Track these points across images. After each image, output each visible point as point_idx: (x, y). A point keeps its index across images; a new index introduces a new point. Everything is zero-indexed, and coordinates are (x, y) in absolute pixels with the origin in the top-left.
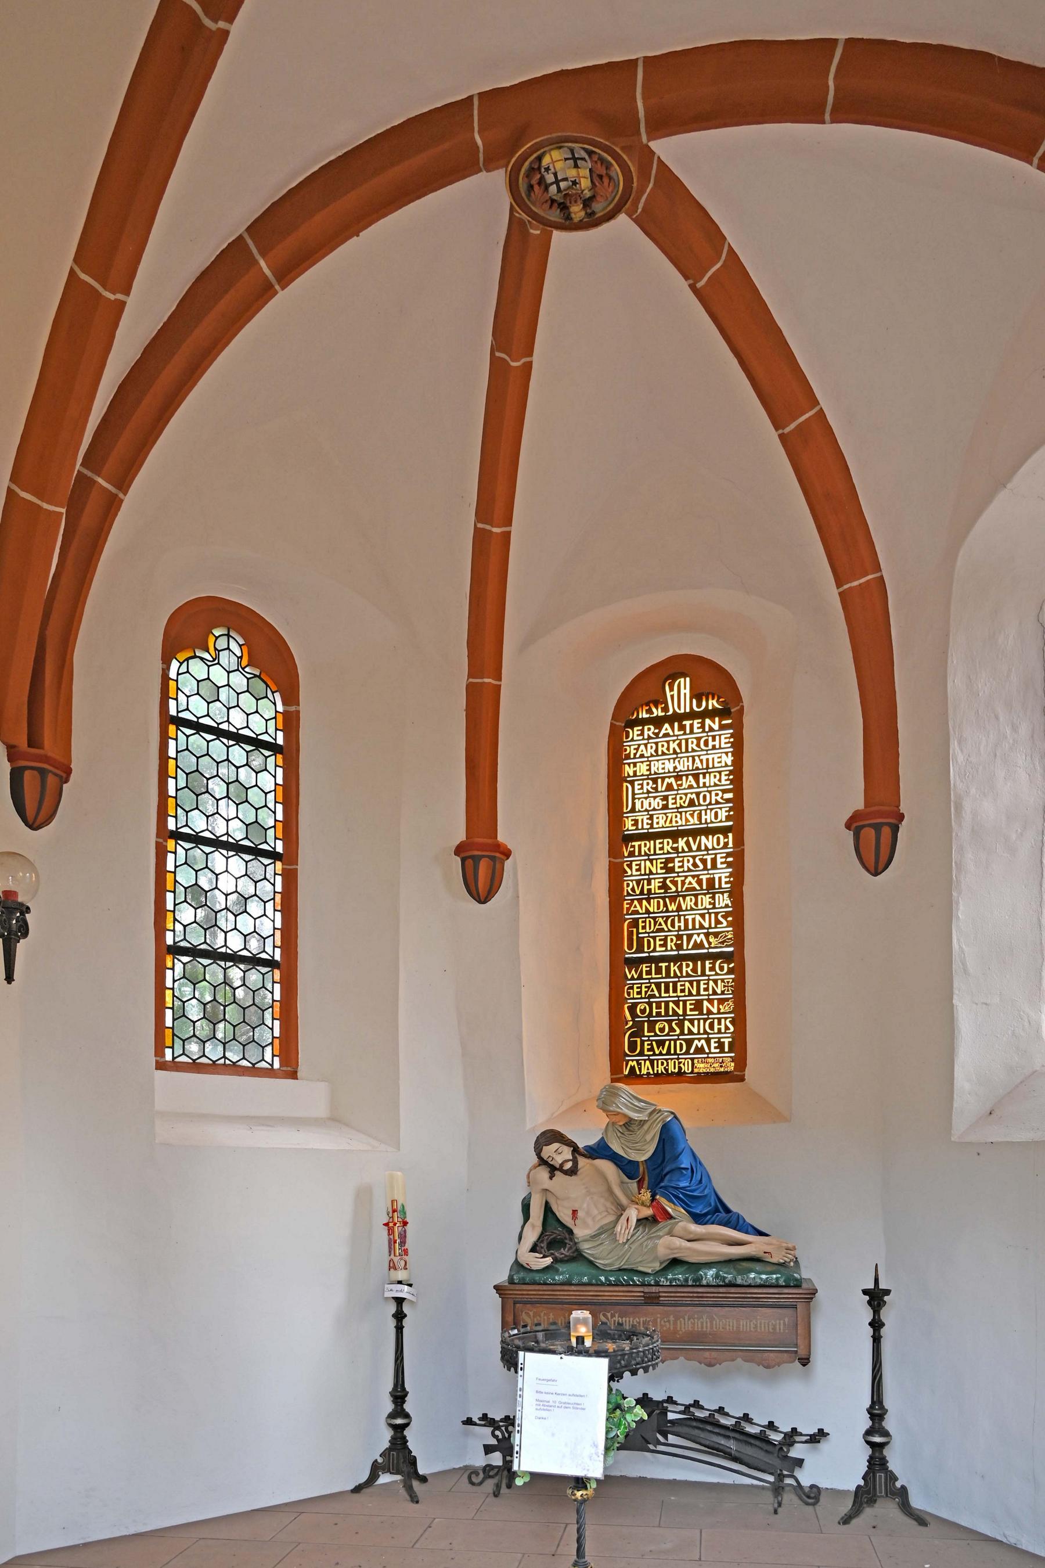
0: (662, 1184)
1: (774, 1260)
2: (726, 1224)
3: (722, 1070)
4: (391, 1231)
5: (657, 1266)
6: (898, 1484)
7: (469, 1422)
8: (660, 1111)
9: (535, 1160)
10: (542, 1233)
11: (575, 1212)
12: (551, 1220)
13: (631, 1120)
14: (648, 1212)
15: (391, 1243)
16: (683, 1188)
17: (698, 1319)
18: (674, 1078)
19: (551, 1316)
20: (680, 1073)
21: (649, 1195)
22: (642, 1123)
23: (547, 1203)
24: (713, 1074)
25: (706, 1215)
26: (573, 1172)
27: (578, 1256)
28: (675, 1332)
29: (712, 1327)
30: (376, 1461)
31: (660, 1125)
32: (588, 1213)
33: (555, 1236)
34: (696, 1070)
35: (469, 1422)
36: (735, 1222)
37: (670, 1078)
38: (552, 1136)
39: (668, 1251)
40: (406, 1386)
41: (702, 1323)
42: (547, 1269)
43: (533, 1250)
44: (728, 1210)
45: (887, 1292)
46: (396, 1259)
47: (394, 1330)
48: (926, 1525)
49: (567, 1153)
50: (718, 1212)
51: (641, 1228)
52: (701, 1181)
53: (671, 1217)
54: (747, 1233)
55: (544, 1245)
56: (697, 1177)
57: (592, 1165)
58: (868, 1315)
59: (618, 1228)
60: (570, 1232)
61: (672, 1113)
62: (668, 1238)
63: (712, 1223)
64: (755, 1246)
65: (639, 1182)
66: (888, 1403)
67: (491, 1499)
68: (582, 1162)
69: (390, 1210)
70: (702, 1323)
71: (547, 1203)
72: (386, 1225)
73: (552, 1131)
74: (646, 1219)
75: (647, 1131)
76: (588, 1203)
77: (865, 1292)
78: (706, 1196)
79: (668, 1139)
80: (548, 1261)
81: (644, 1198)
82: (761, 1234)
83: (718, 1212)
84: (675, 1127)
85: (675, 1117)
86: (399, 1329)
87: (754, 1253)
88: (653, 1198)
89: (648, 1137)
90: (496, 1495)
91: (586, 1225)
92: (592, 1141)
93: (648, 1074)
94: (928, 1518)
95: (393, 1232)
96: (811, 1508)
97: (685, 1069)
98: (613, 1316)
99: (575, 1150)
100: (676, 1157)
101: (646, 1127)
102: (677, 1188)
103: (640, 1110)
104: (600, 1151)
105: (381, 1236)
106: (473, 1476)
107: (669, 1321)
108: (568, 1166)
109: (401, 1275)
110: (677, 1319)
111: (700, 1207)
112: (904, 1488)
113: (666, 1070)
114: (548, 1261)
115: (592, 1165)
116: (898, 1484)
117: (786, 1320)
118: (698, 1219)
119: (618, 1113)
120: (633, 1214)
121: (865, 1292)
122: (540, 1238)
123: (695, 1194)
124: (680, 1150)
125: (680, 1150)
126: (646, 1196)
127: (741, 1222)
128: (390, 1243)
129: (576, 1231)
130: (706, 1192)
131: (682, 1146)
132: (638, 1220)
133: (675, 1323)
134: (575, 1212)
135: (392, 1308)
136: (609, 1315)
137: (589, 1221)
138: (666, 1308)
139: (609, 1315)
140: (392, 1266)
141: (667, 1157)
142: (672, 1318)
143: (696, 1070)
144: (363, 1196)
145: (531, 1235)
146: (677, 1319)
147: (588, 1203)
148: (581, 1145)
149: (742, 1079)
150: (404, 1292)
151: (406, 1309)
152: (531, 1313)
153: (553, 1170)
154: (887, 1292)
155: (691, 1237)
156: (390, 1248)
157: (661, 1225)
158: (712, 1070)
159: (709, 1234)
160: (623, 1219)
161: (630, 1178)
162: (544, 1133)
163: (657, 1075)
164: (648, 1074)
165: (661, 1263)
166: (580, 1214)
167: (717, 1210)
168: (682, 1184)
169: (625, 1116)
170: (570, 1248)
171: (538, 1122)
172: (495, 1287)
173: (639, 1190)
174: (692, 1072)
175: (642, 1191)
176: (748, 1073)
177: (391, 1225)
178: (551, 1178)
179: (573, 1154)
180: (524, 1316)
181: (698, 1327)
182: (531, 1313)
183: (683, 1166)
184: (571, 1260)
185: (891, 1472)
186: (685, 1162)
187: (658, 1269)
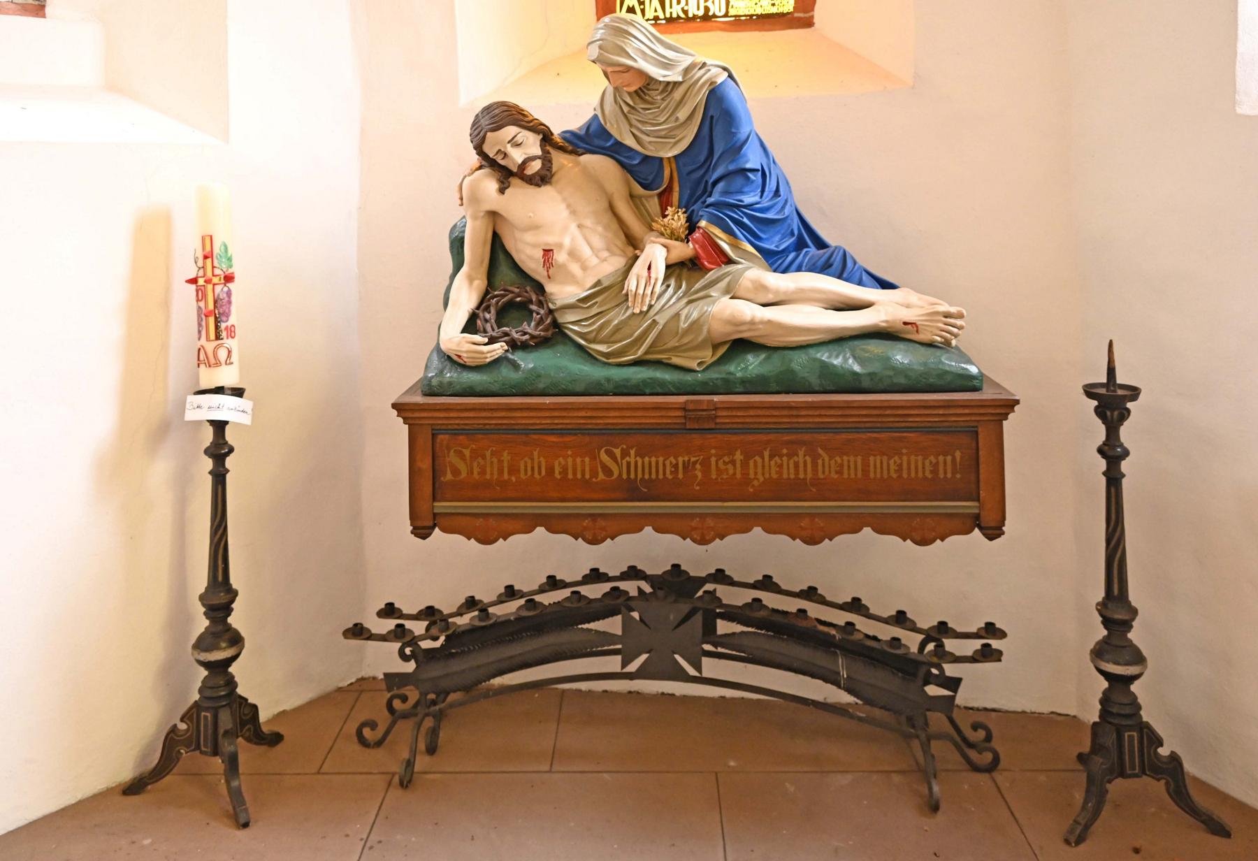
0: (711, 200)
1: (922, 337)
2: (825, 268)
4: (201, 295)
5: (708, 356)
6: (1163, 751)
7: (358, 632)
9: (474, 159)
10: (487, 293)
11: (547, 252)
12: (505, 273)
14: (683, 250)
15: (202, 315)
16: (748, 206)
17: (790, 456)
19: (506, 456)
20: (707, 17)
21: (683, 218)
22: (670, 86)
24: (760, 17)
25: (785, 252)
26: (542, 179)
27: (555, 335)
28: (746, 481)
29: (815, 470)
30: (175, 726)
32: (573, 254)
33: (511, 293)
34: (732, 12)
35: (358, 632)
36: (837, 264)
37: (692, 25)
40: (232, 581)
41: (796, 465)
42: (496, 362)
43: (470, 326)
45: (1134, 393)
46: (210, 347)
47: (209, 480)
48: (1227, 835)
49: (532, 145)
50: (803, 246)
51: (672, 282)
52: (777, 193)
53: (730, 261)
54: (860, 283)
55: (490, 316)
58: (1099, 432)
59: (631, 284)
60: (540, 288)
61: (725, 69)
63: (799, 269)
64: (885, 309)
65: (660, 195)
66: (1135, 595)
67: (395, 793)
68: (559, 159)
69: (200, 255)
70: (796, 465)
72: (193, 281)
73: (503, 104)
75: (681, 102)
76: (567, 235)
77: (1090, 391)
79: (718, 114)
80: (499, 348)
81: (675, 225)
83: (803, 246)
84: (731, 92)
85: (730, 76)
86: (219, 477)
88: (692, 227)
89: (682, 114)
90: (406, 783)
91: (572, 279)
92: (576, 122)
94: (1225, 816)
95: (205, 296)
96: (983, 778)
98: (625, 454)
99: (546, 137)
100: (736, 149)
102: (738, 207)
103: (667, 65)
104: (591, 139)
105: (185, 302)
106: (367, 732)
107: (733, 462)
108: (536, 166)
109: (227, 376)
110: (747, 457)
111: (777, 238)
112: (1174, 758)
113: (686, 12)
114: (499, 348)
115: (585, 170)
116: (1163, 751)
117: (958, 454)
118: (775, 260)
119: (629, 69)
120: (656, 254)
121: (1090, 391)
122: (483, 303)
123: (770, 215)
124: (742, 136)
125: (742, 136)
126: (677, 219)
127: (849, 264)
128: (199, 316)
129: (550, 288)
130: (787, 211)
132: (668, 267)
133: (745, 464)
134: (547, 252)
135: (208, 435)
136: (618, 452)
137: (575, 268)
138: (727, 438)
139: (618, 452)
140: (204, 360)
141: (719, 149)
142: (738, 456)
143: (732, 12)
144: (151, 231)
145: (465, 297)
146: (747, 457)
148: (557, 130)
149: (808, 23)
150: (225, 408)
151: (230, 436)
152: (467, 452)
153: (505, 175)
154: (1134, 393)
155: (770, 298)
156: (200, 325)
157: (710, 276)
159: (802, 290)
160: (639, 268)
161: (645, 187)
162: (487, 109)
163: (670, 20)
167: (800, 245)
169: (641, 73)
171: (479, 93)
172: (394, 406)
174: (726, 15)
175: (670, 210)
176: (819, 14)
177: (201, 282)
178: (502, 191)
180: (453, 458)
181: (789, 473)
182: (467, 452)
183: (748, 166)
184: (542, 343)
185: (1148, 726)
186: (753, 159)
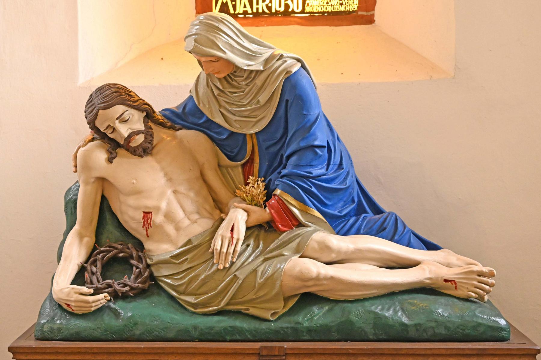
3: (342, 9)
5: (281, 308)
8: (282, 56)
9: (88, 132)
10: (94, 249)
11: (147, 214)
13: (236, 69)
14: (262, 214)
16: (316, 177)
18: (280, 18)
20: (287, 13)
21: (262, 185)
22: (253, 74)
23: (104, 198)
26: (144, 151)
27: (151, 287)
31: (282, 78)
34: (308, 9)
37: (274, 19)
38: (111, 95)
39: (299, 283)
43: (79, 278)
44: (377, 210)
49: (137, 121)
50: (360, 212)
53: (300, 225)
54: (409, 245)
55: (97, 269)
56: (336, 159)
57: (175, 137)
60: (140, 246)
61: (299, 60)
62: (296, 258)
63: (358, 232)
64: (431, 266)
68: (161, 134)
71: (104, 198)
73: (114, 86)
74: (260, 226)
76: (163, 197)
78: (349, 187)
80: (102, 298)
81: (255, 192)
82: (430, 246)
84: (304, 80)
85: (303, 66)
87: (421, 282)
88: (269, 195)
89: (263, 98)
91: (168, 239)
93: (245, 13)
97: (293, 7)
99: (149, 115)
101: (259, 81)
104: (187, 117)
113: (269, 8)
118: (339, 225)
120: (239, 218)
122: (90, 258)
123: (334, 185)
124: (312, 118)
125: (312, 118)
129: (148, 245)
130: (348, 182)
131: (314, 113)
132: (248, 229)
134: (147, 214)
137: (170, 229)
143: (308, 9)
145: (75, 253)
147: (163, 197)
148: (158, 108)
149: (370, 20)
153: (114, 146)
155: (333, 257)
157: (284, 237)
158: (329, 9)
159: (359, 251)
160: (224, 230)
163: (257, 15)
164: (245, 13)
165: (286, 300)
166: (158, 219)
167: (359, 211)
168: (316, 172)
169: (229, 63)
170: (140, 274)
171: (96, 70)
173: (246, 178)
174: (303, 12)
175: (251, 179)
176: (379, 12)
178: (110, 160)
179: (145, 123)
183: (317, 143)
184: (140, 293)
187: (281, 312)
